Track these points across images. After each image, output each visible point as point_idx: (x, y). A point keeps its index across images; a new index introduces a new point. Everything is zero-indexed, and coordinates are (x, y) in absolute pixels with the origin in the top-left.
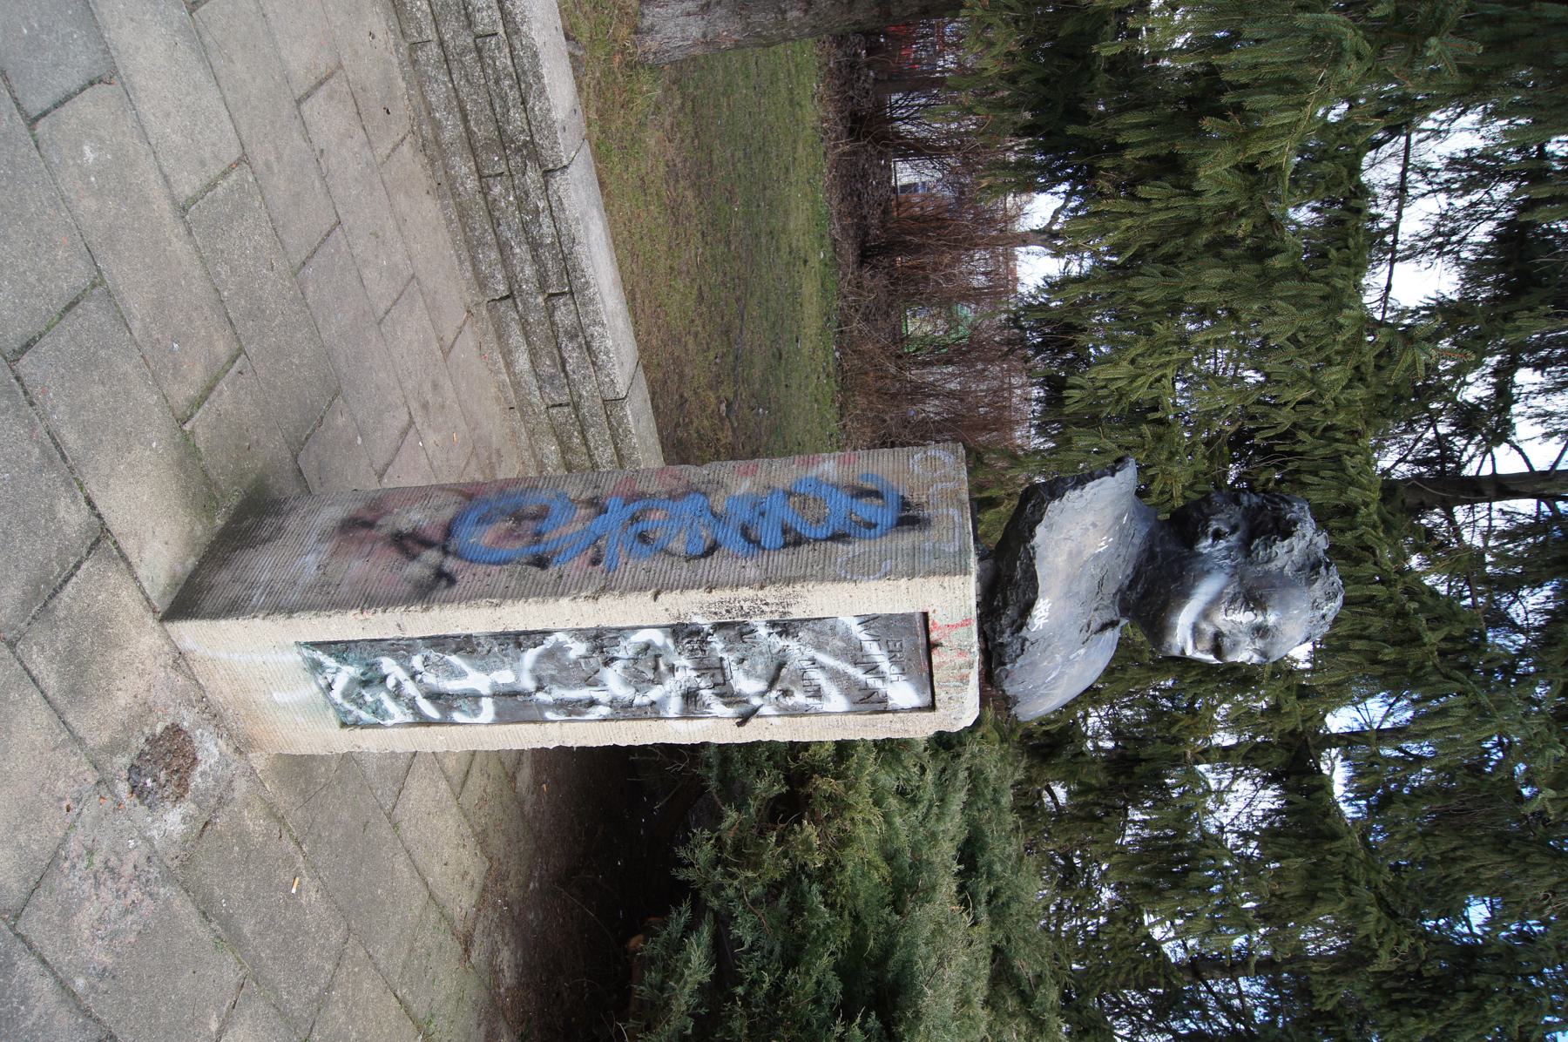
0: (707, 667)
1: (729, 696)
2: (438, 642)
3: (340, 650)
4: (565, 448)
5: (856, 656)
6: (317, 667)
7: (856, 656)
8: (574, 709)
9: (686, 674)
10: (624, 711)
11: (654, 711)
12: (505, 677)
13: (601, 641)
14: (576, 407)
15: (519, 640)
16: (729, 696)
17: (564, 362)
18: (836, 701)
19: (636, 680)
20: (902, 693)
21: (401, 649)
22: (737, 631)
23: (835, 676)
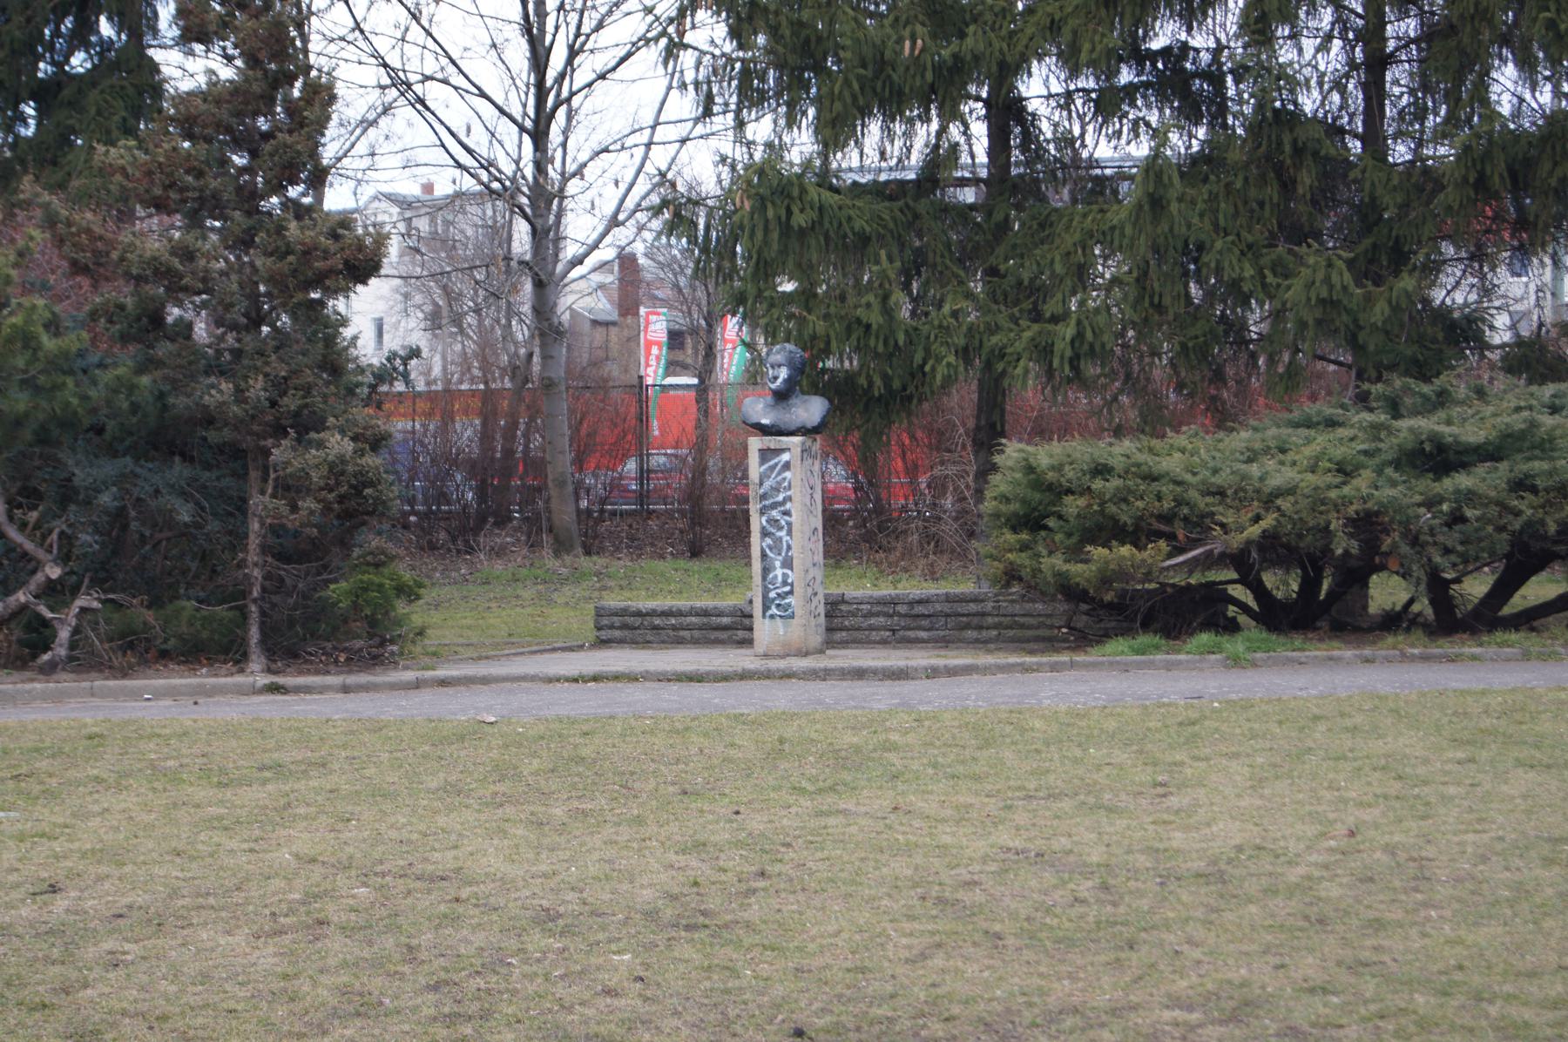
0: (774, 506)
1: (783, 503)
2: (764, 578)
3: (766, 608)
4: (967, 626)
5: (772, 468)
6: (772, 617)
7: (772, 468)
8: (789, 547)
9: (775, 513)
10: (790, 533)
11: (789, 524)
12: (778, 564)
13: (765, 534)
14: (947, 615)
15: (764, 555)
16: (783, 503)
17: (924, 615)
18: (788, 474)
19: (781, 528)
20: (785, 457)
21: (766, 591)
22: (763, 497)
23: (779, 474)
